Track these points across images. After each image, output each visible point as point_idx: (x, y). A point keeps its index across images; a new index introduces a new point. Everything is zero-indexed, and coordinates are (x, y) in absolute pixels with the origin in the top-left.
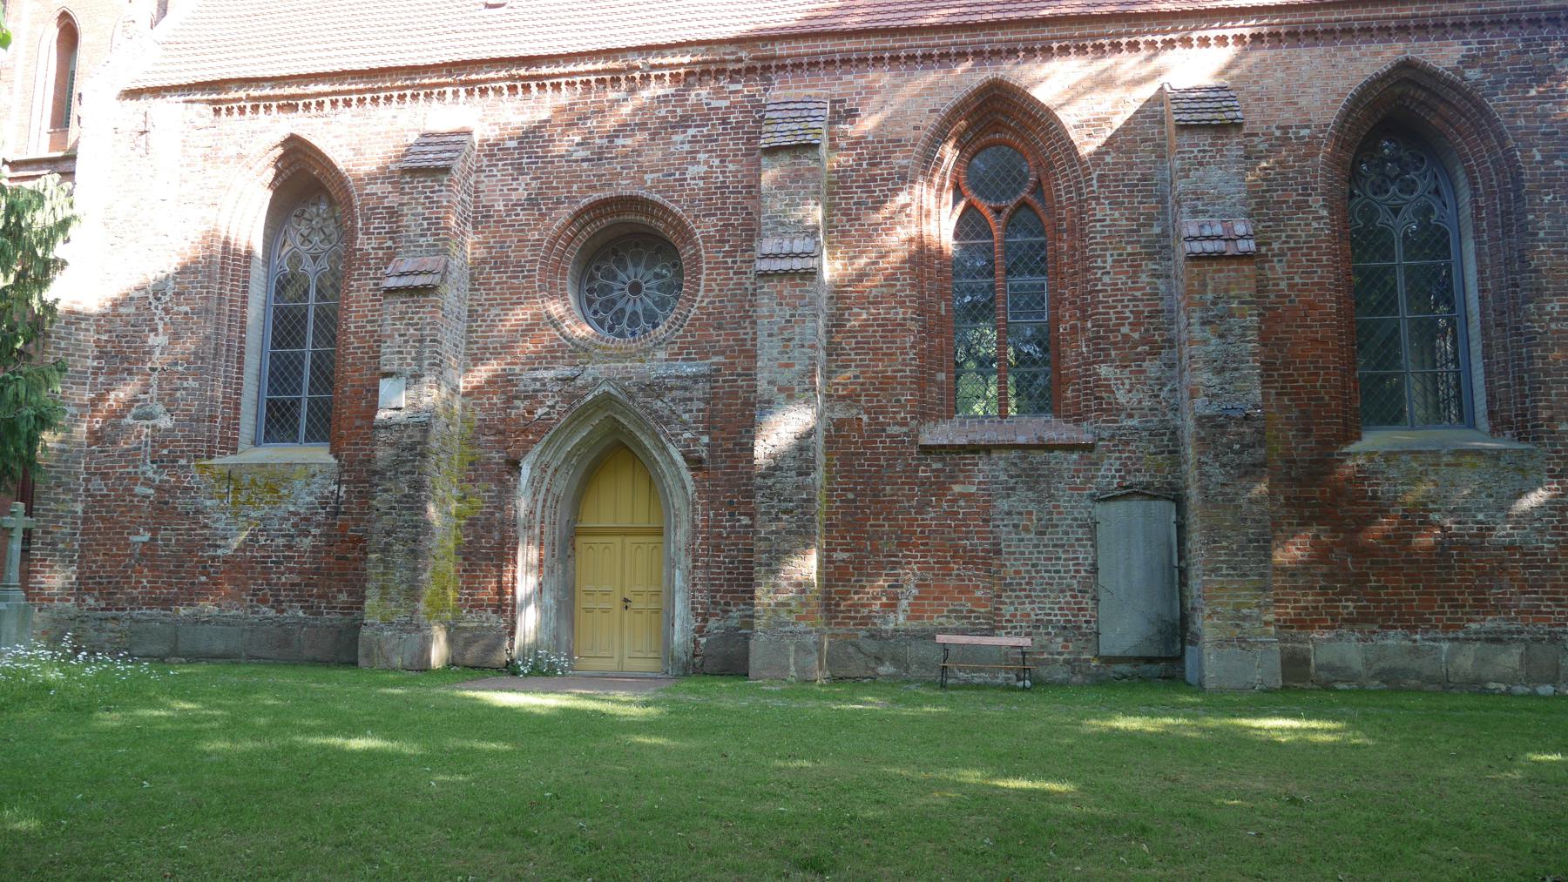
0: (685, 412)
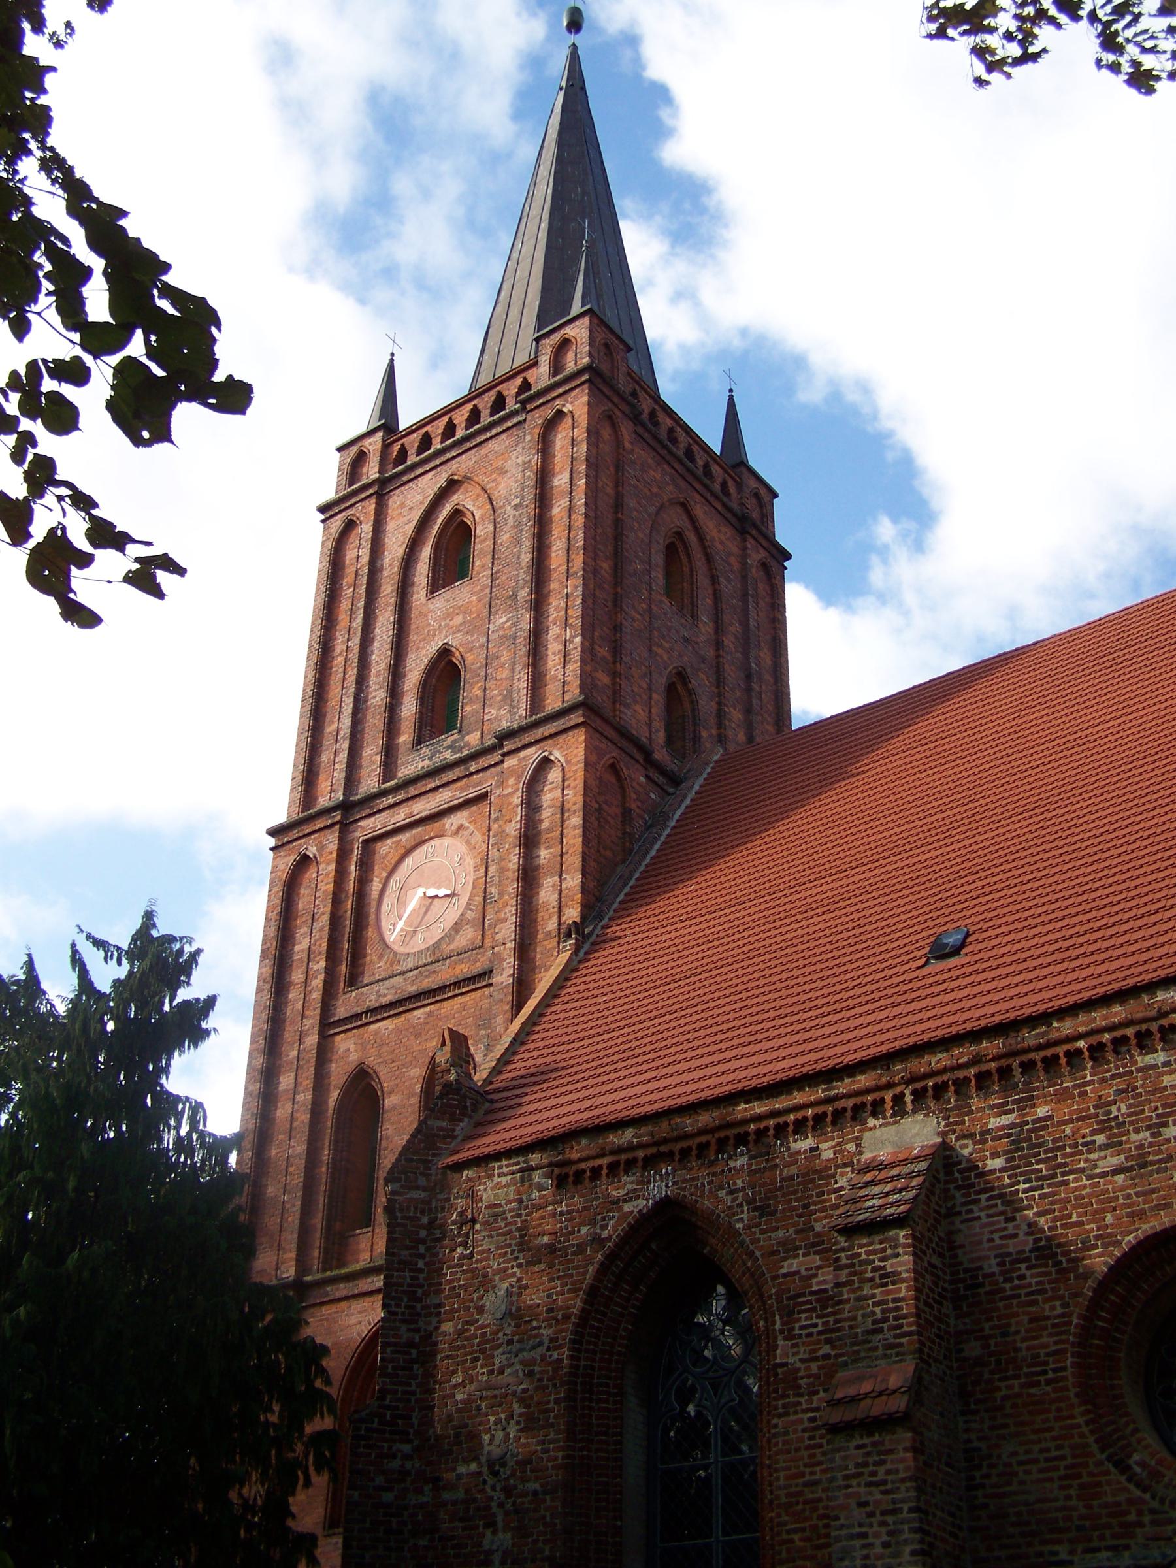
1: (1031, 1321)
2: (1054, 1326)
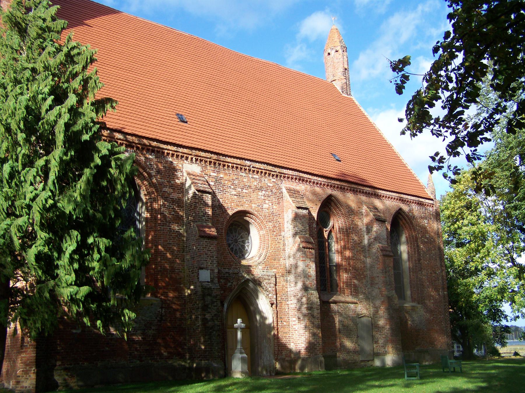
0: (270, 287)
1: (217, 220)
2: (221, 223)
